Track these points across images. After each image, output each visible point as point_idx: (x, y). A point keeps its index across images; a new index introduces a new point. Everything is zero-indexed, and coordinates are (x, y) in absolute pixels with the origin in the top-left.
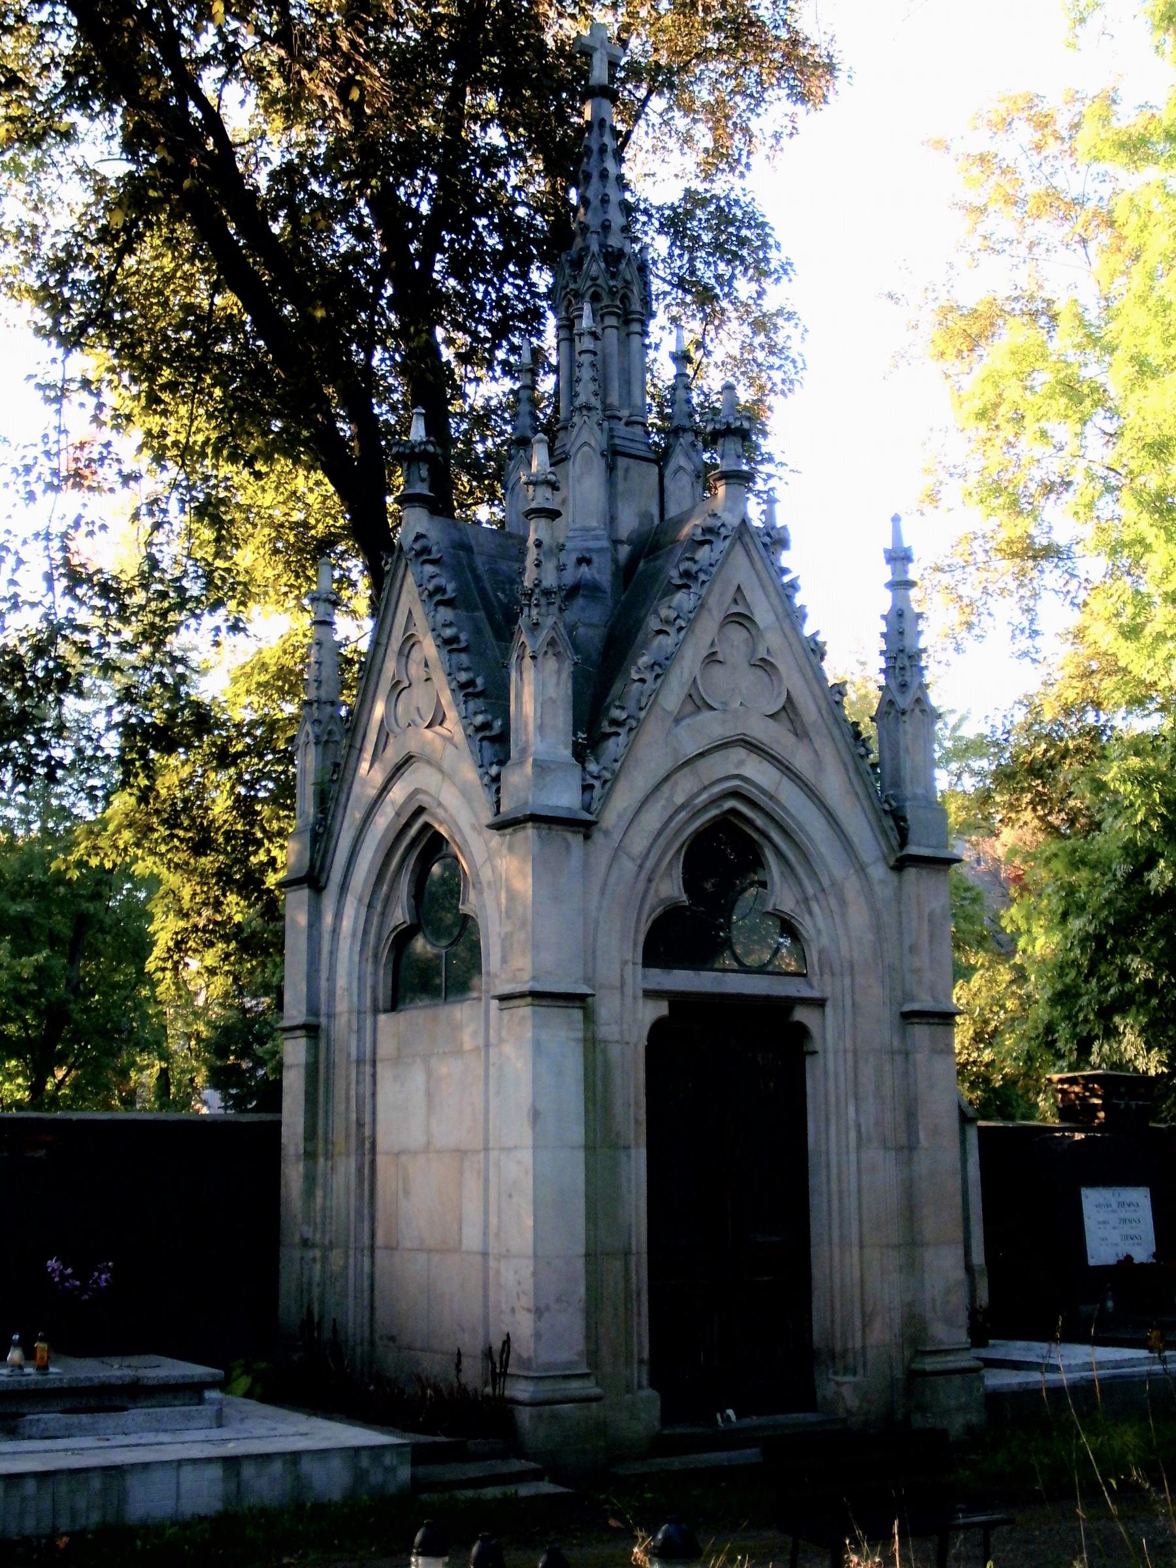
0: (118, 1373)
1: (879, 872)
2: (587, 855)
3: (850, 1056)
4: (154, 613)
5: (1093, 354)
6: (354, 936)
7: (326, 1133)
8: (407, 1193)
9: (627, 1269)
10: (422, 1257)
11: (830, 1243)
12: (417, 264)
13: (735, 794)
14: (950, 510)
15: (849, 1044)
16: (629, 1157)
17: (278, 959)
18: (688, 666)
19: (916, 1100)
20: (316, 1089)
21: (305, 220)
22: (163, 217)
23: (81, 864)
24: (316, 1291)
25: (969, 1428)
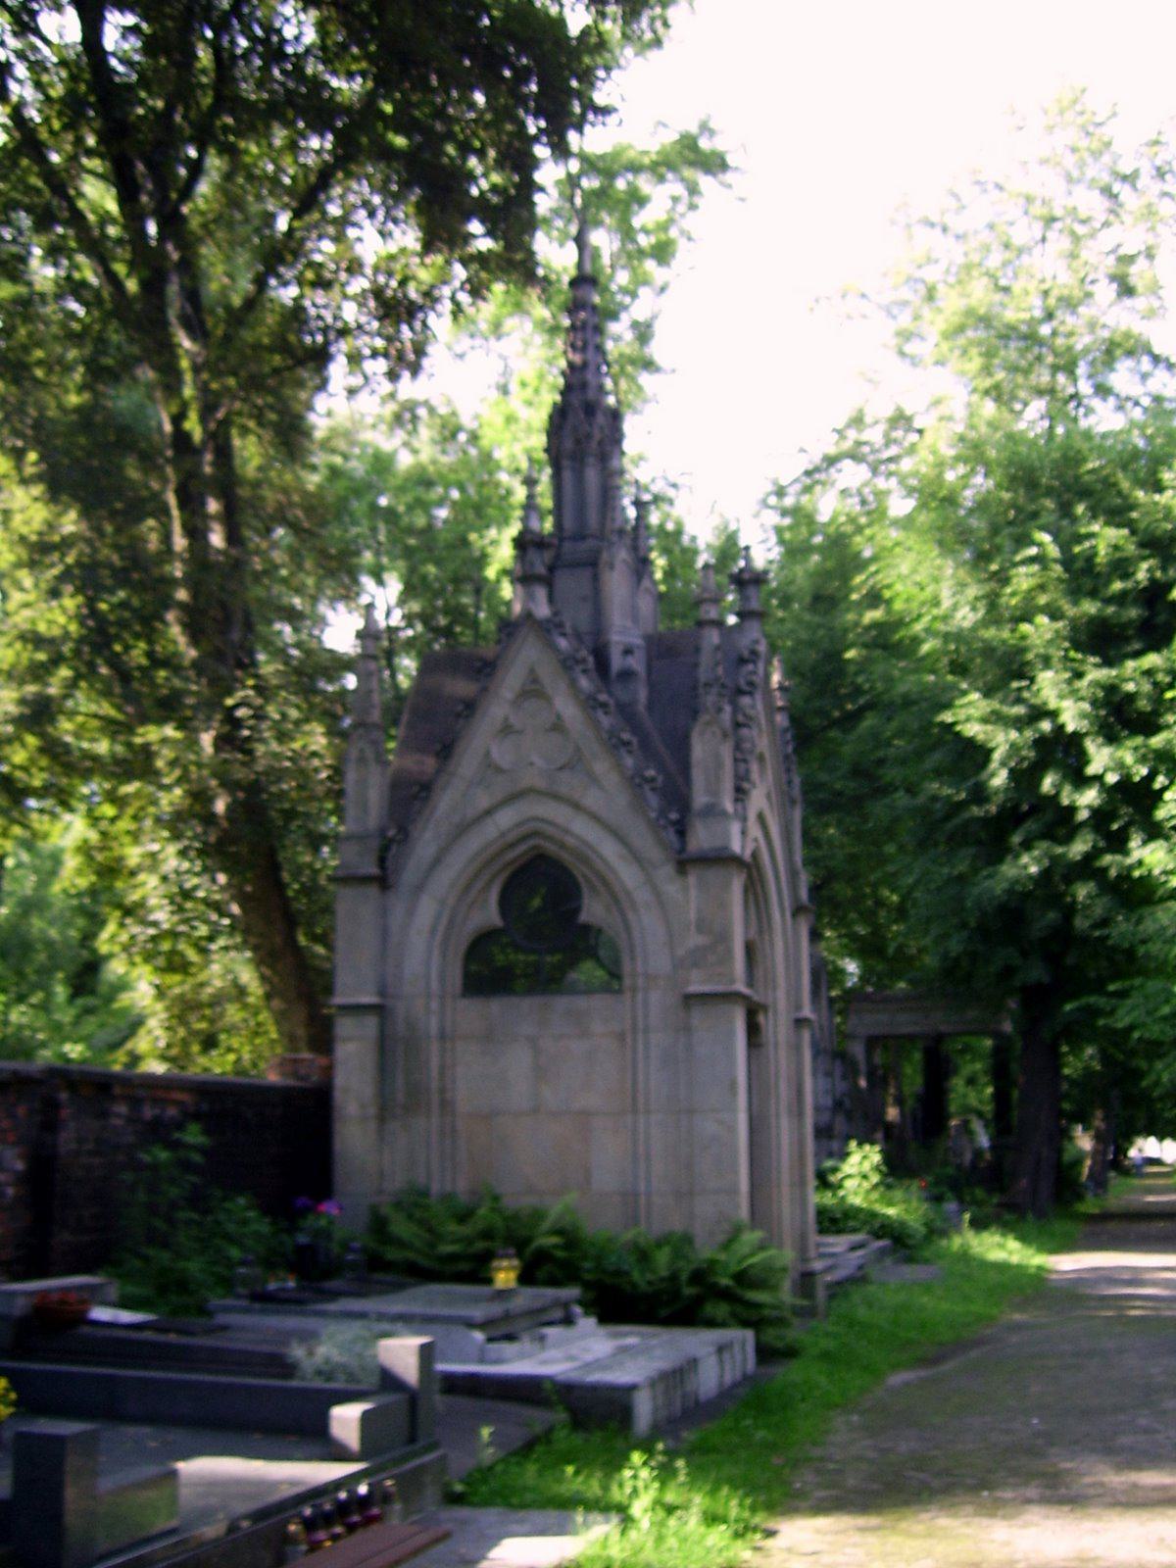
0: (945, 1306)
1: (666, 871)
2: (384, 912)
3: (641, 1106)
4: (1075, 381)
5: (751, 591)
6: (433, 931)
7: (442, 1091)
8: (786, 757)
9: (489, 812)
10: (1068, 321)
11: (776, 1044)
12: (467, 63)
13: (535, 834)
14: (742, 200)
15: (642, 1119)
16: (1131, 1028)
17: (924, 705)
18: (567, 708)
19: (510, 1506)
20: (753, 1144)
21: (912, 1075)
22: (83, 88)
23: (1092, 326)
24: (642, 1200)
25: (844, 1155)
